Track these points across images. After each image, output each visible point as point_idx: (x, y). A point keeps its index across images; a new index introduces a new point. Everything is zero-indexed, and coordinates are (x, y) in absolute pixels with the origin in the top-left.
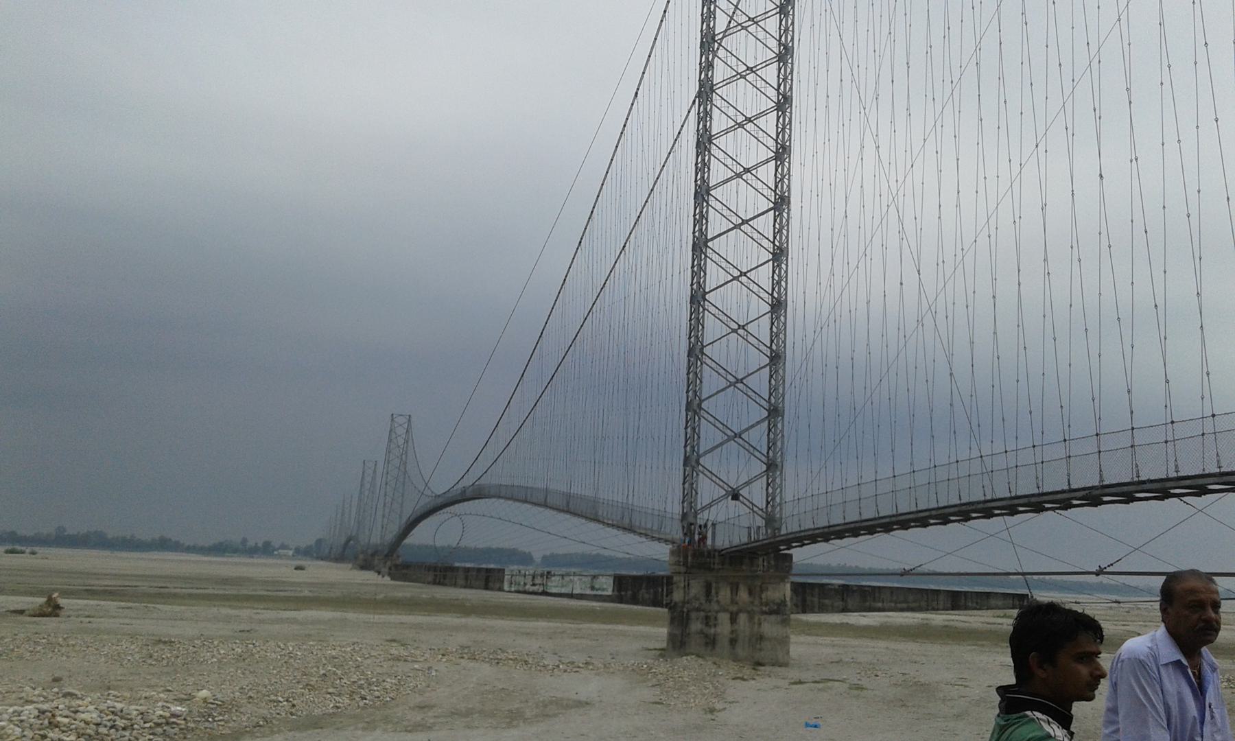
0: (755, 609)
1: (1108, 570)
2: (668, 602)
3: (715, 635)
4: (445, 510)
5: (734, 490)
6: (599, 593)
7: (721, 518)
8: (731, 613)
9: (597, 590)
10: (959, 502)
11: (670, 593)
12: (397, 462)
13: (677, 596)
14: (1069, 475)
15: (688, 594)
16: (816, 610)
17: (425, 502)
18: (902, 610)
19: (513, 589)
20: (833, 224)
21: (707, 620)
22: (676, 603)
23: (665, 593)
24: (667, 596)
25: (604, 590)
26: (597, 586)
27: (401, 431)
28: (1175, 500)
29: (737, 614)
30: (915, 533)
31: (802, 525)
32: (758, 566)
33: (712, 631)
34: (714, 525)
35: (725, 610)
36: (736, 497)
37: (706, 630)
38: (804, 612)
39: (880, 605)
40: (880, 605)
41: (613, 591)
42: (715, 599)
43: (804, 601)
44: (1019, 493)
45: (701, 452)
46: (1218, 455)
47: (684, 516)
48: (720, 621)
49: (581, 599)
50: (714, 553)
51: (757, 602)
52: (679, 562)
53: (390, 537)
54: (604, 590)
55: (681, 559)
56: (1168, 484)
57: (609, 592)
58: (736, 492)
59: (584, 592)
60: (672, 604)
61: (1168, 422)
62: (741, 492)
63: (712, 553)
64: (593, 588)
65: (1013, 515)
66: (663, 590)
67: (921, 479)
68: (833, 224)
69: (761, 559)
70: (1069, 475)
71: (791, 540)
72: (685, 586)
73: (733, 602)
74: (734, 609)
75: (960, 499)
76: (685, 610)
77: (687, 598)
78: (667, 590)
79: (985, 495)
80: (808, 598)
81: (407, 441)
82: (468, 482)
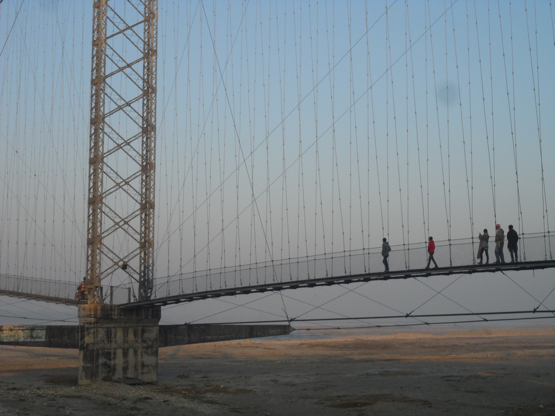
0: (139, 345)
1: (297, 319)
2: (82, 344)
3: (114, 365)
6: (37, 340)
8: (124, 349)
9: (35, 338)
10: (364, 273)
11: (83, 338)
13: (88, 339)
14: (451, 259)
15: (97, 337)
20: (176, 89)
21: (108, 355)
22: (88, 345)
23: (80, 338)
24: (81, 340)
25: (39, 338)
26: (35, 335)
29: (128, 349)
33: (112, 362)
35: (120, 348)
36: (125, 267)
37: (108, 362)
38: (166, 345)
39: (209, 337)
40: (209, 337)
41: (46, 338)
42: (114, 340)
46: (211, 284)
48: (117, 356)
50: (112, 307)
51: (140, 340)
54: (39, 338)
57: (43, 340)
58: (125, 263)
59: (26, 340)
61: (222, 267)
62: (128, 263)
63: (113, 308)
64: (32, 337)
66: (78, 336)
68: (176, 89)
70: (451, 259)
71: (165, 302)
72: (94, 332)
73: (125, 341)
75: (258, 283)
76: (95, 349)
77: (96, 340)
78: (81, 335)
79: (241, 284)
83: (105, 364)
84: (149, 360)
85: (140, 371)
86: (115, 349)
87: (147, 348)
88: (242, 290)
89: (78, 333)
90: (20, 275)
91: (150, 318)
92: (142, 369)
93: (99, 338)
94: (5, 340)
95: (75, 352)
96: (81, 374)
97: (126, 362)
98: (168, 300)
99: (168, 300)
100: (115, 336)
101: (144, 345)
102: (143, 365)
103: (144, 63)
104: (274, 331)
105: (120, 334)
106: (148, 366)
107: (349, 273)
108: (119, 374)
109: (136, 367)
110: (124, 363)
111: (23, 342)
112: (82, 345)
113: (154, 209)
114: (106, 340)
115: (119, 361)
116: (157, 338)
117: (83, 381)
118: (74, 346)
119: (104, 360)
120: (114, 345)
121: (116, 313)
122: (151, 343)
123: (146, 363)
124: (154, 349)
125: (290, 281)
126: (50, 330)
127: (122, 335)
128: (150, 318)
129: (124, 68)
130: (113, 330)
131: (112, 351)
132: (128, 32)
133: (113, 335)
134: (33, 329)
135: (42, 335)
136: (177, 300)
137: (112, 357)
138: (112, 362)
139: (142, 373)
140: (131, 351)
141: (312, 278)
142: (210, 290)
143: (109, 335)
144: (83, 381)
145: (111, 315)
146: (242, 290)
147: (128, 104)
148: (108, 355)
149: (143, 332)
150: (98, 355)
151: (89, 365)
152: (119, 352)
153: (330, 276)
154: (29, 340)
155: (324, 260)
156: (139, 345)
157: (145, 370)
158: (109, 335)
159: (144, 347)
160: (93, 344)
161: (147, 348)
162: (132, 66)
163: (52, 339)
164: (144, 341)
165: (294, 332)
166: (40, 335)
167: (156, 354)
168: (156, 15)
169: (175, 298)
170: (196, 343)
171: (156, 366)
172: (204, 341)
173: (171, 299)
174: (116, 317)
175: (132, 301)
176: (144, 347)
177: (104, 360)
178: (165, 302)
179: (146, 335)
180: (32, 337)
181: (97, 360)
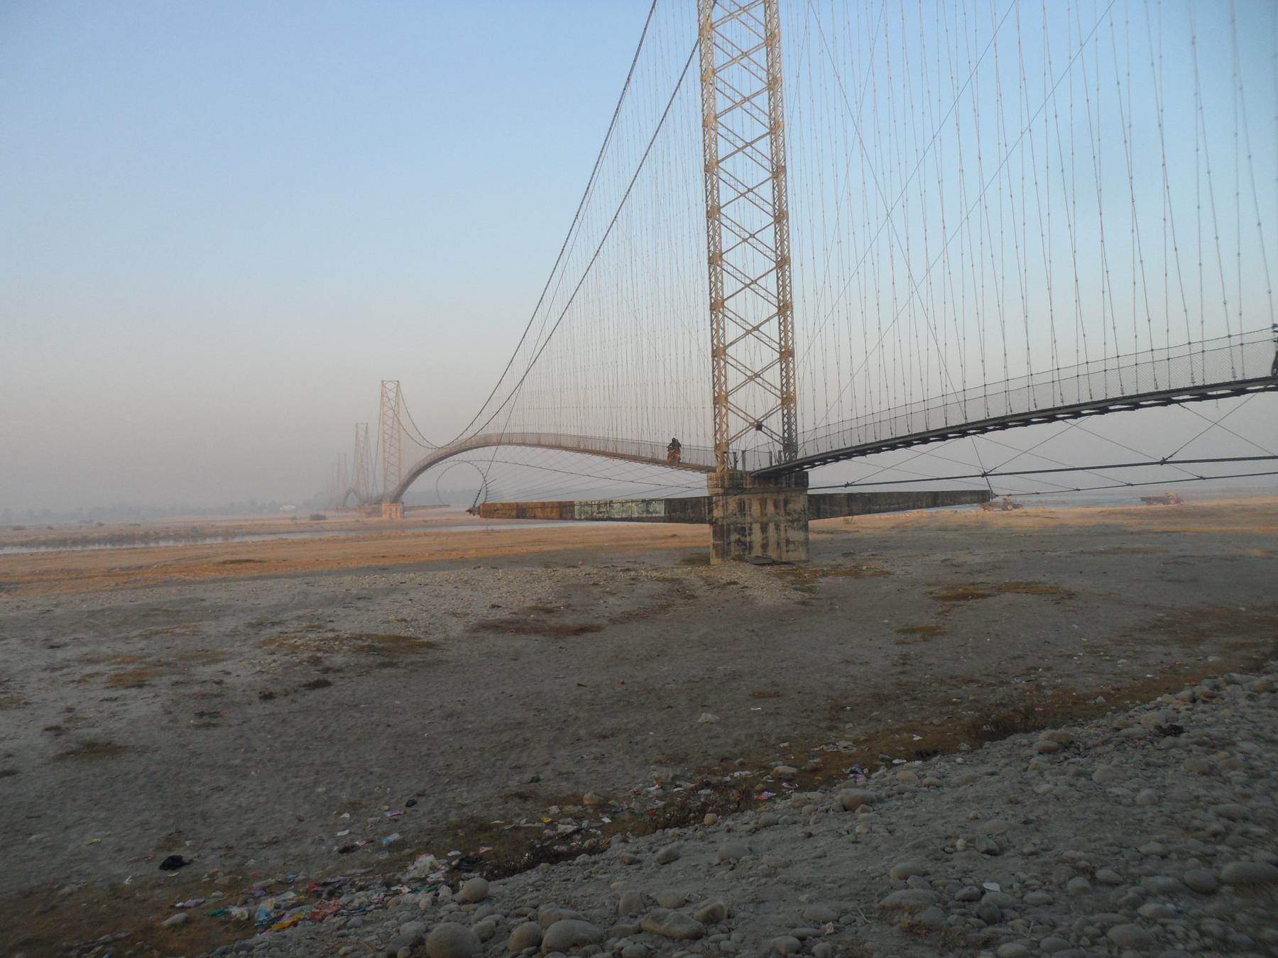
0: (781, 518)
3: (750, 542)
4: (447, 459)
5: (757, 421)
6: (654, 515)
7: (751, 447)
8: (762, 524)
9: (652, 513)
11: (711, 511)
12: (391, 413)
13: (717, 513)
16: (828, 515)
17: (422, 455)
18: (895, 510)
19: (583, 517)
22: (717, 519)
24: (709, 514)
26: (651, 510)
27: (391, 395)
28: (1176, 405)
30: (871, 457)
31: (894, 433)
32: (782, 483)
33: (748, 539)
34: (743, 452)
35: (757, 522)
36: (759, 427)
37: (743, 539)
38: (819, 518)
39: (878, 507)
40: (878, 507)
43: (818, 509)
44: (898, 436)
45: (729, 389)
47: (717, 447)
49: (935, 505)
50: (743, 474)
51: (782, 512)
52: (717, 485)
53: (393, 487)
55: (720, 482)
56: (1007, 420)
59: (641, 516)
60: (714, 520)
64: (648, 512)
65: (1004, 429)
66: (705, 510)
67: (821, 433)
69: (784, 477)
71: (812, 462)
73: (763, 514)
74: (765, 519)
76: (725, 523)
80: (822, 506)
81: (397, 395)
82: (470, 434)
83: (738, 542)
84: (796, 535)
85: (784, 548)
86: (751, 524)
87: (793, 521)
88: (1233, 387)
89: (704, 506)
90: (620, 437)
91: (793, 486)
92: (787, 546)
93: (730, 511)
94: (616, 517)
95: (706, 529)
96: (713, 553)
97: (766, 538)
98: (949, 431)
99: (949, 431)
100: (750, 508)
101: (788, 518)
102: (788, 542)
103: (780, 319)
104: (968, 499)
105: (756, 508)
106: (794, 542)
107: (1241, 375)
108: (757, 551)
109: (778, 544)
110: (763, 539)
111: (638, 517)
112: (710, 520)
113: (793, 357)
114: (738, 513)
115: (756, 537)
116: (804, 510)
117: (715, 561)
118: (702, 521)
119: (737, 537)
120: (748, 519)
121: (748, 482)
122: (797, 516)
123: (791, 540)
124: (801, 523)
125: (1152, 390)
126: (670, 503)
127: (759, 507)
128: (793, 486)
129: (744, 147)
130: (747, 502)
131: (747, 526)
132: (748, 150)
133: (747, 506)
134: (648, 502)
135: (660, 509)
136: (824, 459)
137: (747, 533)
138: (748, 539)
139: (787, 551)
140: (771, 526)
141: (1199, 383)
142: (1060, 405)
143: (742, 508)
144: (715, 561)
145: (742, 484)
146: (1233, 387)
147: (754, 282)
148: (742, 531)
149: (786, 502)
150: (729, 531)
151: (719, 542)
152: (756, 527)
153: (1239, 378)
154: (644, 515)
155: (1151, 364)
156: (781, 518)
157: (791, 547)
158: (742, 508)
159: (789, 521)
160: (723, 518)
161: (793, 521)
162: (760, 329)
163: (673, 514)
164: (789, 514)
165: (995, 500)
166: (658, 509)
167: (805, 528)
168: (781, 125)
169: (957, 429)
170: (857, 514)
171: (806, 543)
172: (869, 512)
173: (954, 430)
174: (748, 487)
175: (774, 464)
176: (789, 521)
177: (737, 537)
178: (812, 462)
179: (791, 506)
180: (648, 512)
181: (729, 536)
